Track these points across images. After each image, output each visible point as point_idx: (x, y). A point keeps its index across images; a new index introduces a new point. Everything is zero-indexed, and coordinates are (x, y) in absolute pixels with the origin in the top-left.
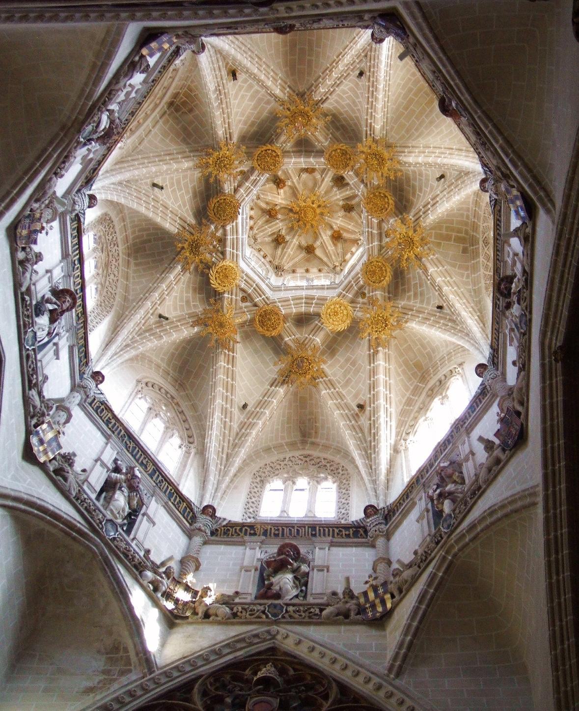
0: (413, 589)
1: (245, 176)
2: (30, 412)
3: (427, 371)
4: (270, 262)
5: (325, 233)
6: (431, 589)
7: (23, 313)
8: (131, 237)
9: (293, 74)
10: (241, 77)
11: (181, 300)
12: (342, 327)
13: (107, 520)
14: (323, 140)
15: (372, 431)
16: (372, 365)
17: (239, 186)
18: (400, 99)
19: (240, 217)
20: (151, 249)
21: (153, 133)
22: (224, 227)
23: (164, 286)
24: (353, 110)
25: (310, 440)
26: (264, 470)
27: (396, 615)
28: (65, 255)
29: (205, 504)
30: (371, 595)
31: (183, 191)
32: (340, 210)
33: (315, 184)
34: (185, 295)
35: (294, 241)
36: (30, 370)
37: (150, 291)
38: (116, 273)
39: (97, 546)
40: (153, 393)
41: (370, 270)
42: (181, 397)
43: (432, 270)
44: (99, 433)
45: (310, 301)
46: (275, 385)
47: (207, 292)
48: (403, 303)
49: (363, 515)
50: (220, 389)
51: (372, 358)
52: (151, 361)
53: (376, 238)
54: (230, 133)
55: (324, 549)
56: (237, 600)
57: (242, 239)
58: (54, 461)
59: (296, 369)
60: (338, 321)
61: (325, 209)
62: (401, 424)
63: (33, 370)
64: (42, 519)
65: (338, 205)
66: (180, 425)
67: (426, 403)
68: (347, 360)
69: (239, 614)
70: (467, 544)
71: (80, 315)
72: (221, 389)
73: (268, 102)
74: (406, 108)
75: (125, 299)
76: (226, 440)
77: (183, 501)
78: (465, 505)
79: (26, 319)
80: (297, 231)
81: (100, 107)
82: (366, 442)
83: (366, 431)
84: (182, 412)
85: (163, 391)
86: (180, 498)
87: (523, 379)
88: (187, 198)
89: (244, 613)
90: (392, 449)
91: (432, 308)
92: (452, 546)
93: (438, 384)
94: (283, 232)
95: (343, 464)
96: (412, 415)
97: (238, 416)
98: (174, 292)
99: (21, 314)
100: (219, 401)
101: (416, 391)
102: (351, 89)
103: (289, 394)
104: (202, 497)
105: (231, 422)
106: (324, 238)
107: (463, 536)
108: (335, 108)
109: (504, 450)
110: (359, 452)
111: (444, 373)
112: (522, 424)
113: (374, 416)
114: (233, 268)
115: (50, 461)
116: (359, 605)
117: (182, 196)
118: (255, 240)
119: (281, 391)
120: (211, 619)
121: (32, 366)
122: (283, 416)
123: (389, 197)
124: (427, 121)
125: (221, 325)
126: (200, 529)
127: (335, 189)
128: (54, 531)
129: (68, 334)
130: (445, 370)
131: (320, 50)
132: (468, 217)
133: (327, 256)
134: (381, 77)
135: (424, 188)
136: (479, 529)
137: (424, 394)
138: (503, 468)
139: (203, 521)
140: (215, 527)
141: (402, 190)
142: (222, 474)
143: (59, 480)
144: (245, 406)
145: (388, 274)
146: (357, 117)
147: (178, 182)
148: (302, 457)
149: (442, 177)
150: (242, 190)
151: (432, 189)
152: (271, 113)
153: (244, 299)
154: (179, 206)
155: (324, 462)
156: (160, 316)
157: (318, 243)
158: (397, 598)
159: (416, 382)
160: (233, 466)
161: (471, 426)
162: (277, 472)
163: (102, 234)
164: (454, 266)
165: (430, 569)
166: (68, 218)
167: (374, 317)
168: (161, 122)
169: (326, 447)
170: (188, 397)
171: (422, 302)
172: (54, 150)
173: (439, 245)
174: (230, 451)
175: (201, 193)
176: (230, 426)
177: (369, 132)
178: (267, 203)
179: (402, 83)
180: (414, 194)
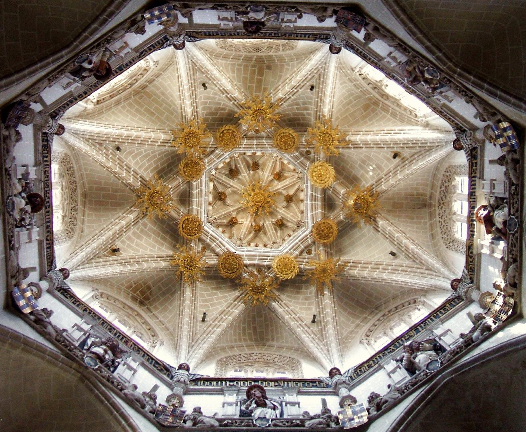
0: (490, 102)
1: (206, 247)
2: (322, 427)
3: (370, 99)
4: (294, 231)
5: (276, 186)
6: (484, 86)
7: (237, 426)
8: (249, 342)
9: (123, 204)
10: (118, 244)
11: (304, 304)
12: (331, 171)
13: (427, 369)
14: (177, 182)
15: (411, 145)
16: (361, 146)
17: (213, 251)
18: (145, 119)
19: (237, 252)
20: (259, 326)
21: (162, 319)
22: (246, 266)
23: (286, 317)
24: (155, 156)
25: (428, 200)
26: (446, 239)
27: (513, 118)
28: (221, 392)
29: (450, 286)
30: (501, 141)
31: (214, 297)
32: (258, 173)
33: (235, 193)
34: (300, 301)
35: (282, 212)
36: (287, 424)
37: (290, 329)
38: (275, 356)
39: (444, 378)
40: (377, 331)
41: (284, 145)
42: (386, 308)
43: (280, 95)
44: (376, 374)
45: (314, 197)
46: (377, 228)
47: (297, 283)
48: (313, 120)
49: (462, 152)
50: (375, 274)
51: (356, 146)
52: (352, 332)
53: (261, 141)
54: (167, 257)
55: (483, 184)
56: (506, 259)
57: (263, 252)
58: (370, 411)
59: (367, 210)
60: (327, 174)
61: (256, 185)
62: (410, 123)
63: (287, 422)
64: (410, 423)
65: (254, 175)
66: (405, 310)
67: (393, 100)
68: (361, 167)
69: (514, 257)
70: (444, 54)
71: (276, 384)
72: (376, 273)
73: (145, 225)
74: (153, 114)
75: (297, 350)
76: (415, 270)
77: (445, 306)
78: (415, 57)
79: (243, 424)
80: (274, 209)
81: (69, 350)
82: (421, 151)
83: (413, 151)
84: (396, 308)
85: (376, 323)
86: (441, 309)
87: (302, 7)
88: (220, 295)
89: (514, 252)
90: (425, 128)
91: (313, 95)
92: (449, 68)
93: (376, 90)
94: (274, 220)
95: (443, 172)
96: (404, 112)
97: (402, 261)
98: (294, 311)
99: (237, 428)
100: (385, 276)
101: (385, 109)
102: (134, 157)
103: (387, 216)
104: (445, 290)
105: (371, 264)
106: (279, 187)
107: (438, 58)
108: (151, 171)
109: (367, 24)
110: (427, 156)
111: (366, 85)
112: (342, 8)
113: (400, 144)
114: (279, 260)
115: (369, 413)
116: (509, 152)
117: (217, 299)
118: (274, 243)
119: (381, 223)
120: (517, 282)
121: (284, 423)
122: (407, 222)
123: (223, 129)
124: (163, 97)
125: (324, 271)
126: (466, 293)
127: (240, 177)
128: (424, 414)
129: (286, 395)
130: (363, 83)
131: (103, 181)
132: (239, 65)
133: (294, 185)
134: (116, 133)
135: (217, 101)
136: (429, 44)
137: (386, 102)
138: (380, 25)
139: (461, 290)
140: (468, 280)
141: (221, 120)
142: (438, 275)
143: (385, 407)
144: (393, 254)
145: (287, 131)
146: (159, 154)
147: (206, 301)
148: (440, 207)
149: (204, 85)
150: (218, 250)
151: (216, 94)
152: (155, 223)
153: (309, 252)
154: (225, 301)
155: (443, 188)
156: (313, 321)
157: (284, 192)
158: (500, 117)
159: (379, 109)
160: (434, 265)
161: (376, 57)
162: (449, 229)
163: (237, 365)
164: (281, 76)
165: (470, 87)
166: (191, 387)
167: (321, 143)
168: (155, 312)
169: (433, 186)
170: (387, 302)
171: (310, 103)
172: (98, 389)
173: (265, 90)
174: (424, 268)
175: (219, 283)
176: (406, 267)
177: (169, 144)
178: (250, 233)
179: (130, 116)
180: (223, 109)
